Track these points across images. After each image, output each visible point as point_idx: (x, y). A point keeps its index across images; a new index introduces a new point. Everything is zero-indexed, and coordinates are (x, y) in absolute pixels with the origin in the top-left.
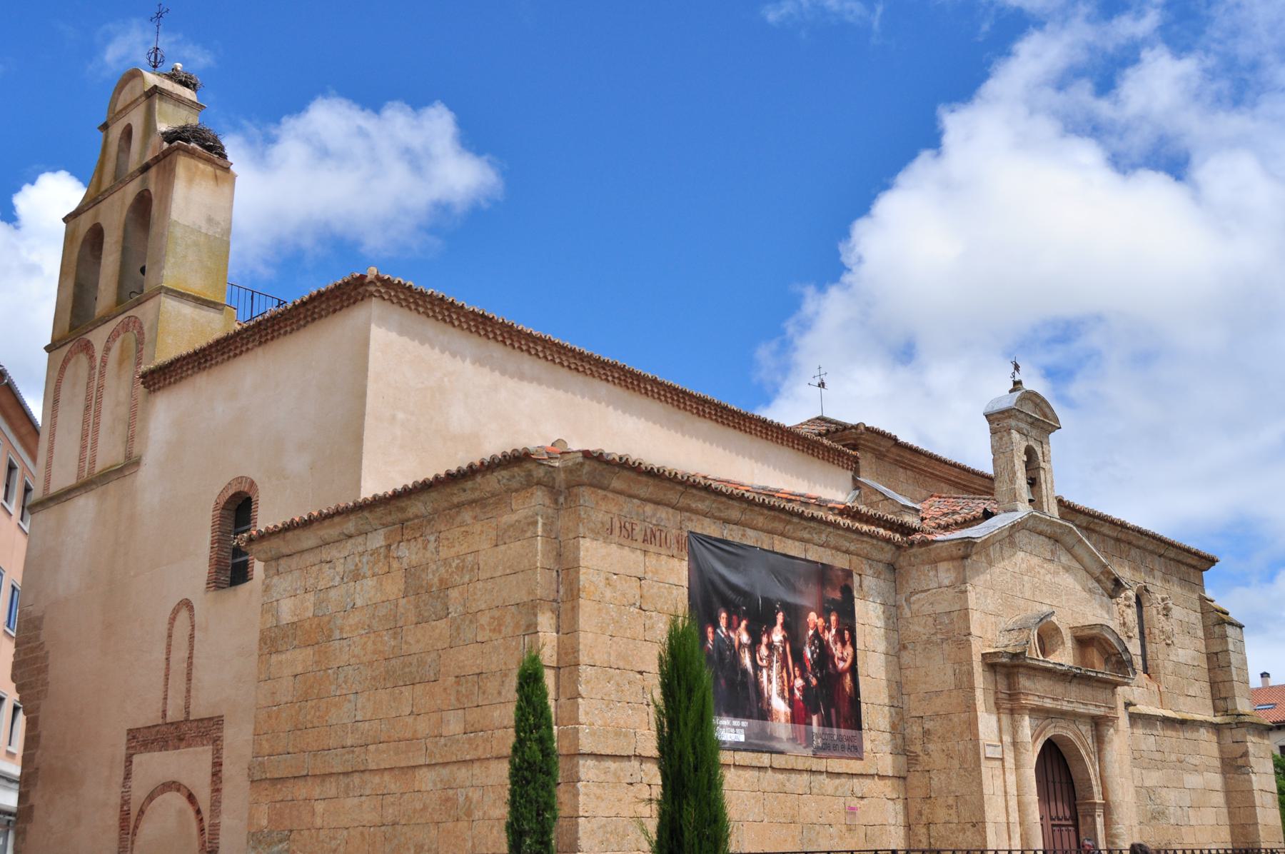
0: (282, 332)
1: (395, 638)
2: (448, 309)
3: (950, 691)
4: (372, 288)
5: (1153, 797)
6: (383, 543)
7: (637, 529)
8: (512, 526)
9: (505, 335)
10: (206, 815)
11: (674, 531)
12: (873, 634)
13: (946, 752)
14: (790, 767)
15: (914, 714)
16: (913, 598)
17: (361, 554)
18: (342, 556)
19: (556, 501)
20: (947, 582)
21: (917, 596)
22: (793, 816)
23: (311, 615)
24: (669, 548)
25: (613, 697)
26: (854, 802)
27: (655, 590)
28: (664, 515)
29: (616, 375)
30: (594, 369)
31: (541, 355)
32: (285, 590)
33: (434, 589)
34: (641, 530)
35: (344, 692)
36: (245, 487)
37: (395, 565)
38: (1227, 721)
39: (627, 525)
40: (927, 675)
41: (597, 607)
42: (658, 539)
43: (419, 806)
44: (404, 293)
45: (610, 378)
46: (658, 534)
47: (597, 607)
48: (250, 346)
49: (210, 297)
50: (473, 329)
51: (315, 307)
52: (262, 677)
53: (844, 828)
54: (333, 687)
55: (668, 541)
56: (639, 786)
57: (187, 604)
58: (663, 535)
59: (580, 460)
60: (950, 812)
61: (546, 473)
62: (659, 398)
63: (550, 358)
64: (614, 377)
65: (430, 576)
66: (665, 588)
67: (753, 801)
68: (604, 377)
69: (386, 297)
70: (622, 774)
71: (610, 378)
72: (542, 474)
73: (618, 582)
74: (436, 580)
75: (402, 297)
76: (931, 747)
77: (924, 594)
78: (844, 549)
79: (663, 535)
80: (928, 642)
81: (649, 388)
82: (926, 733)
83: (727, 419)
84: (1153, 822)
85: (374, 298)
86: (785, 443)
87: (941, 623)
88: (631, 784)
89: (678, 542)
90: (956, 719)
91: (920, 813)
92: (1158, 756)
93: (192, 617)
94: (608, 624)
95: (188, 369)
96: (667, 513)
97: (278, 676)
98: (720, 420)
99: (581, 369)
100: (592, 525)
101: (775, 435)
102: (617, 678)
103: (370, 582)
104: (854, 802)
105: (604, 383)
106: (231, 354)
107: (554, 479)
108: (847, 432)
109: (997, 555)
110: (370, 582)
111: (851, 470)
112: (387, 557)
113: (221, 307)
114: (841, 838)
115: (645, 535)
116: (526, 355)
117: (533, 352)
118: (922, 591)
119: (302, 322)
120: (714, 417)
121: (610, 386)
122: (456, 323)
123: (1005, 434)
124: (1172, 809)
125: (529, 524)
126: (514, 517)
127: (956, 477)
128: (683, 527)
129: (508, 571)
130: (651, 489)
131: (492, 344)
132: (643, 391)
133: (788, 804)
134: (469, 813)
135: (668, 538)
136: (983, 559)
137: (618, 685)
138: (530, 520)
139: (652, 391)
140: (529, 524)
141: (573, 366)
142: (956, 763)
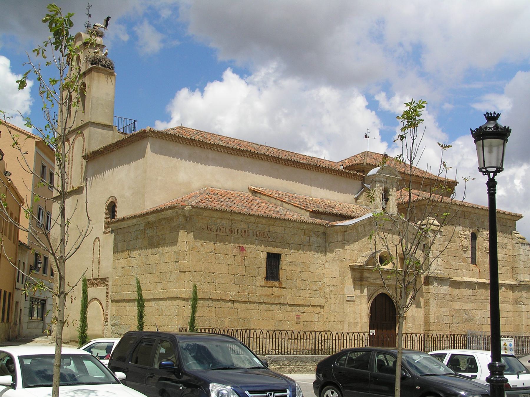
0: (124, 145)
1: (146, 259)
2: (177, 138)
3: (338, 277)
4: (148, 134)
5: (467, 313)
6: (143, 228)
7: (214, 228)
8: (174, 227)
9: (201, 144)
10: (105, 309)
11: (228, 227)
12: (313, 257)
13: (335, 298)
14: (272, 302)
15: (328, 285)
16: (330, 245)
17: (138, 231)
18: (133, 231)
19: (187, 220)
20: (340, 240)
21: (331, 244)
22: (272, 318)
23: (126, 249)
24: (226, 233)
25: (202, 281)
26: (299, 314)
27: (220, 247)
28: (225, 222)
29: (248, 154)
30: (238, 153)
31: (216, 150)
32: (119, 240)
33: (155, 245)
34: (216, 228)
35: (134, 274)
36: (113, 200)
37: (146, 236)
38: (515, 284)
39: (210, 226)
40: (332, 271)
41: (197, 253)
42: (222, 230)
43: (151, 311)
44: (160, 134)
45: (245, 155)
46: (222, 229)
47: (197, 253)
48: (115, 149)
49: (107, 123)
50: (188, 144)
51: (132, 139)
52: (114, 267)
53: (294, 322)
54: (131, 272)
55: (226, 231)
56: (211, 308)
57: (97, 238)
58: (224, 229)
59: (191, 208)
60: (335, 318)
61: (182, 212)
62: (268, 160)
63: (219, 150)
64: (247, 155)
65: (155, 240)
66: (224, 246)
67: (256, 313)
68: (243, 155)
69: (154, 136)
70: (205, 304)
71: (245, 155)
72: (181, 212)
73: (205, 245)
74: (156, 241)
75: (160, 136)
76: (332, 296)
77: (333, 243)
78: (301, 228)
79: (224, 229)
80: (333, 260)
81: (263, 157)
82: (331, 291)
83: (296, 165)
84: (466, 323)
85: (149, 137)
86: (327, 173)
87: (337, 254)
88: (209, 307)
89: (230, 231)
90: (339, 287)
91: (327, 318)
92: (473, 297)
93: (99, 241)
94: (202, 259)
95: (97, 155)
96: (226, 221)
97: (117, 267)
98: (296, 166)
99: (233, 153)
100: (196, 228)
101: (322, 170)
102: (204, 275)
103: (140, 240)
104: (299, 314)
105: (243, 157)
106: (109, 151)
107: (185, 213)
108: (359, 165)
109: (362, 229)
110: (140, 240)
111: (361, 180)
112: (144, 233)
113: (111, 127)
114: (293, 325)
115: (217, 229)
116: (210, 150)
117: (212, 149)
118: (333, 242)
119: (129, 143)
120: (293, 165)
121: (246, 158)
122: (181, 142)
123: (374, 183)
124: (478, 318)
125: (178, 227)
126: (175, 224)
127: (415, 180)
128: (232, 226)
129: (173, 241)
130: (219, 215)
131: (196, 148)
132: (260, 159)
133: (271, 314)
134: (162, 314)
135: (226, 229)
136: (354, 231)
137: (205, 277)
138: (178, 226)
139: (264, 158)
140: (178, 227)
141: (229, 153)
142: (338, 302)
